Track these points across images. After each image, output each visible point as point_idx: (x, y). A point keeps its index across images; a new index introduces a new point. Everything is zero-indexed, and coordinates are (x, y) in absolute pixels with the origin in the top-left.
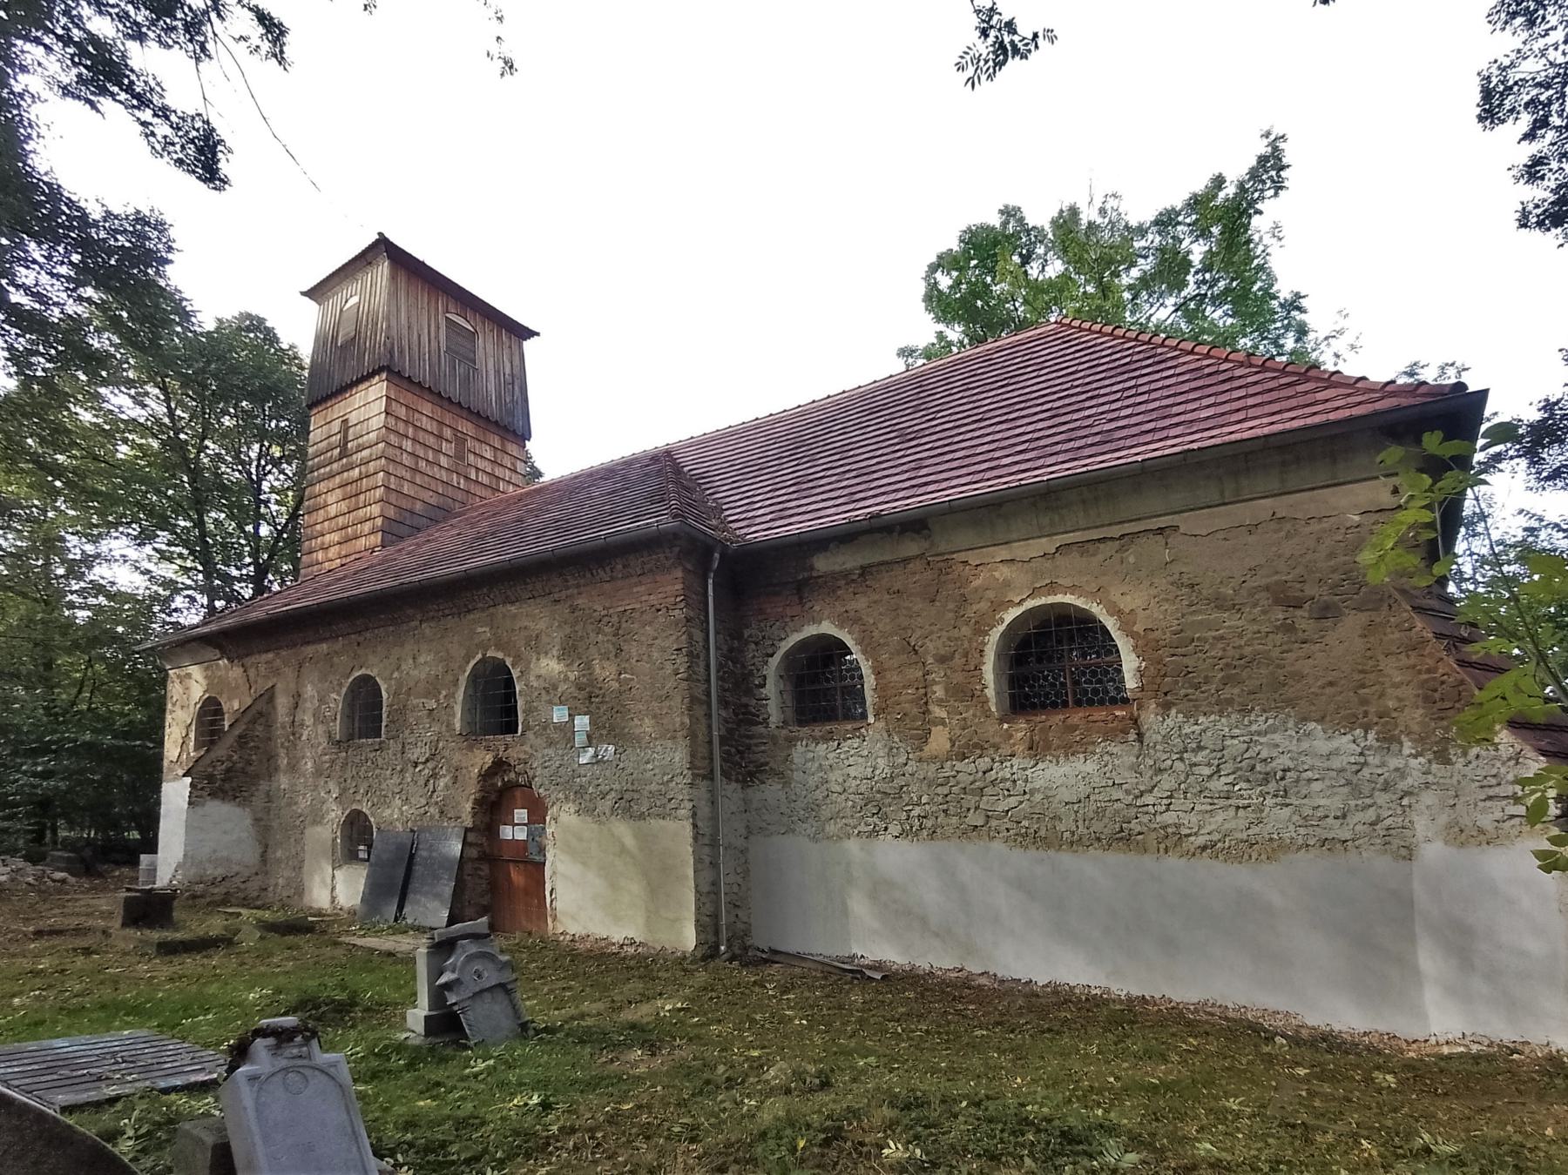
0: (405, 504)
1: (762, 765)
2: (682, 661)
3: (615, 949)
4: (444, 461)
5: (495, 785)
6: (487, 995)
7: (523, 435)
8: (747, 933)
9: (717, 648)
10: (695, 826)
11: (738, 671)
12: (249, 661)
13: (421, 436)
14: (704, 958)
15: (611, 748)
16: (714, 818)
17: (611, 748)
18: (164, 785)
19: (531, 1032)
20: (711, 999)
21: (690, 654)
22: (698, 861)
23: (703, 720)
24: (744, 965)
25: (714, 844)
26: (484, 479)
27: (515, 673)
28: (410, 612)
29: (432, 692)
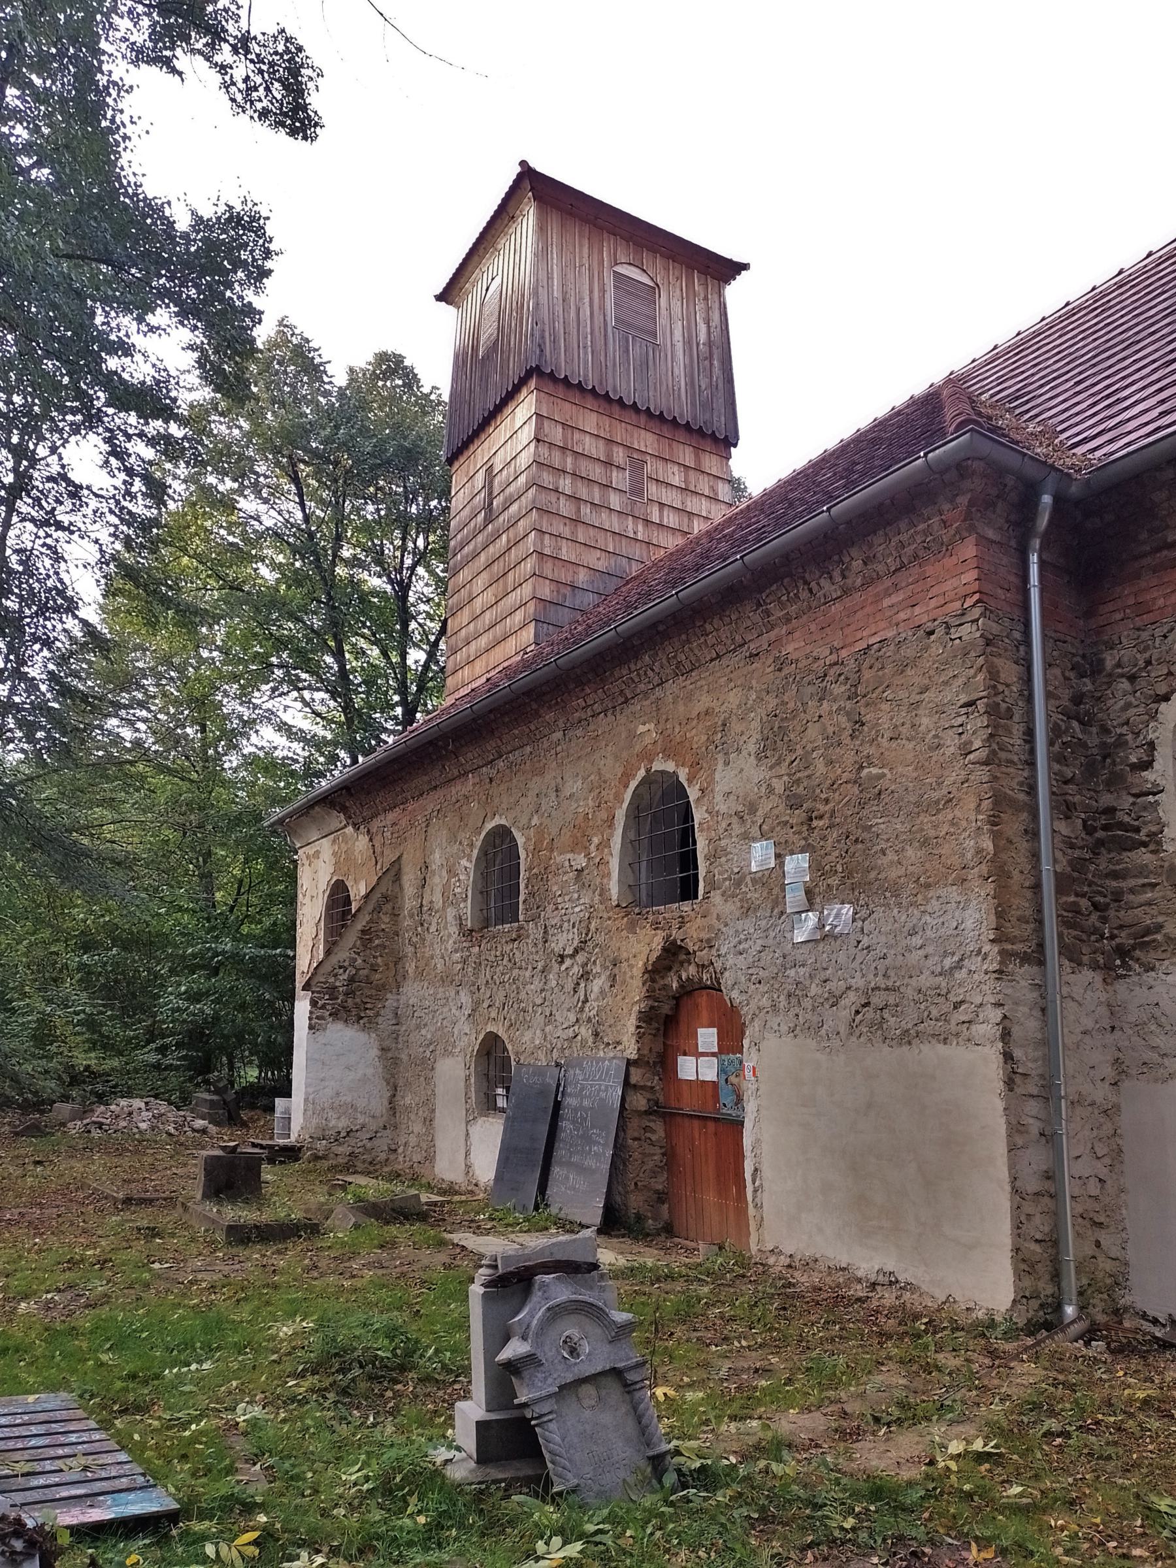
0: (564, 576)
1: (1148, 931)
2: (977, 723)
3: (859, 1291)
4: (615, 501)
5: (666, 987)
6: (588, 1390)
7: (726, 441)
8: (1118, 1281)
9: (1049, 695)
10: (1008, 1056)
11: (1093, 741)
12: (375, 824)
13: (585, 468)
14: (1032, 1328)
15: (847, 910)
16: (1047, 1042)
17: (847, 910)
18: (296, 1003)
19: (670, 1479)
20: (1049, 1434)
21: (993, 711)
22: (1016, 1128)
23: (1024, 845)
24: (1120, 1350)
25: (1048, 1094)
26: (671, 519)
27: (693, 794)
28: (550, 717)
29: (579, 844)
